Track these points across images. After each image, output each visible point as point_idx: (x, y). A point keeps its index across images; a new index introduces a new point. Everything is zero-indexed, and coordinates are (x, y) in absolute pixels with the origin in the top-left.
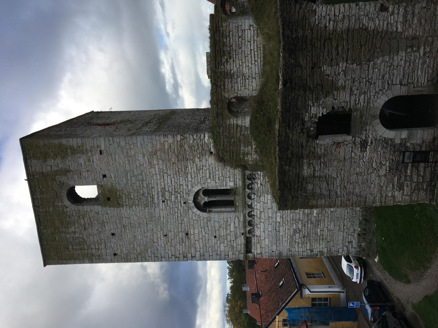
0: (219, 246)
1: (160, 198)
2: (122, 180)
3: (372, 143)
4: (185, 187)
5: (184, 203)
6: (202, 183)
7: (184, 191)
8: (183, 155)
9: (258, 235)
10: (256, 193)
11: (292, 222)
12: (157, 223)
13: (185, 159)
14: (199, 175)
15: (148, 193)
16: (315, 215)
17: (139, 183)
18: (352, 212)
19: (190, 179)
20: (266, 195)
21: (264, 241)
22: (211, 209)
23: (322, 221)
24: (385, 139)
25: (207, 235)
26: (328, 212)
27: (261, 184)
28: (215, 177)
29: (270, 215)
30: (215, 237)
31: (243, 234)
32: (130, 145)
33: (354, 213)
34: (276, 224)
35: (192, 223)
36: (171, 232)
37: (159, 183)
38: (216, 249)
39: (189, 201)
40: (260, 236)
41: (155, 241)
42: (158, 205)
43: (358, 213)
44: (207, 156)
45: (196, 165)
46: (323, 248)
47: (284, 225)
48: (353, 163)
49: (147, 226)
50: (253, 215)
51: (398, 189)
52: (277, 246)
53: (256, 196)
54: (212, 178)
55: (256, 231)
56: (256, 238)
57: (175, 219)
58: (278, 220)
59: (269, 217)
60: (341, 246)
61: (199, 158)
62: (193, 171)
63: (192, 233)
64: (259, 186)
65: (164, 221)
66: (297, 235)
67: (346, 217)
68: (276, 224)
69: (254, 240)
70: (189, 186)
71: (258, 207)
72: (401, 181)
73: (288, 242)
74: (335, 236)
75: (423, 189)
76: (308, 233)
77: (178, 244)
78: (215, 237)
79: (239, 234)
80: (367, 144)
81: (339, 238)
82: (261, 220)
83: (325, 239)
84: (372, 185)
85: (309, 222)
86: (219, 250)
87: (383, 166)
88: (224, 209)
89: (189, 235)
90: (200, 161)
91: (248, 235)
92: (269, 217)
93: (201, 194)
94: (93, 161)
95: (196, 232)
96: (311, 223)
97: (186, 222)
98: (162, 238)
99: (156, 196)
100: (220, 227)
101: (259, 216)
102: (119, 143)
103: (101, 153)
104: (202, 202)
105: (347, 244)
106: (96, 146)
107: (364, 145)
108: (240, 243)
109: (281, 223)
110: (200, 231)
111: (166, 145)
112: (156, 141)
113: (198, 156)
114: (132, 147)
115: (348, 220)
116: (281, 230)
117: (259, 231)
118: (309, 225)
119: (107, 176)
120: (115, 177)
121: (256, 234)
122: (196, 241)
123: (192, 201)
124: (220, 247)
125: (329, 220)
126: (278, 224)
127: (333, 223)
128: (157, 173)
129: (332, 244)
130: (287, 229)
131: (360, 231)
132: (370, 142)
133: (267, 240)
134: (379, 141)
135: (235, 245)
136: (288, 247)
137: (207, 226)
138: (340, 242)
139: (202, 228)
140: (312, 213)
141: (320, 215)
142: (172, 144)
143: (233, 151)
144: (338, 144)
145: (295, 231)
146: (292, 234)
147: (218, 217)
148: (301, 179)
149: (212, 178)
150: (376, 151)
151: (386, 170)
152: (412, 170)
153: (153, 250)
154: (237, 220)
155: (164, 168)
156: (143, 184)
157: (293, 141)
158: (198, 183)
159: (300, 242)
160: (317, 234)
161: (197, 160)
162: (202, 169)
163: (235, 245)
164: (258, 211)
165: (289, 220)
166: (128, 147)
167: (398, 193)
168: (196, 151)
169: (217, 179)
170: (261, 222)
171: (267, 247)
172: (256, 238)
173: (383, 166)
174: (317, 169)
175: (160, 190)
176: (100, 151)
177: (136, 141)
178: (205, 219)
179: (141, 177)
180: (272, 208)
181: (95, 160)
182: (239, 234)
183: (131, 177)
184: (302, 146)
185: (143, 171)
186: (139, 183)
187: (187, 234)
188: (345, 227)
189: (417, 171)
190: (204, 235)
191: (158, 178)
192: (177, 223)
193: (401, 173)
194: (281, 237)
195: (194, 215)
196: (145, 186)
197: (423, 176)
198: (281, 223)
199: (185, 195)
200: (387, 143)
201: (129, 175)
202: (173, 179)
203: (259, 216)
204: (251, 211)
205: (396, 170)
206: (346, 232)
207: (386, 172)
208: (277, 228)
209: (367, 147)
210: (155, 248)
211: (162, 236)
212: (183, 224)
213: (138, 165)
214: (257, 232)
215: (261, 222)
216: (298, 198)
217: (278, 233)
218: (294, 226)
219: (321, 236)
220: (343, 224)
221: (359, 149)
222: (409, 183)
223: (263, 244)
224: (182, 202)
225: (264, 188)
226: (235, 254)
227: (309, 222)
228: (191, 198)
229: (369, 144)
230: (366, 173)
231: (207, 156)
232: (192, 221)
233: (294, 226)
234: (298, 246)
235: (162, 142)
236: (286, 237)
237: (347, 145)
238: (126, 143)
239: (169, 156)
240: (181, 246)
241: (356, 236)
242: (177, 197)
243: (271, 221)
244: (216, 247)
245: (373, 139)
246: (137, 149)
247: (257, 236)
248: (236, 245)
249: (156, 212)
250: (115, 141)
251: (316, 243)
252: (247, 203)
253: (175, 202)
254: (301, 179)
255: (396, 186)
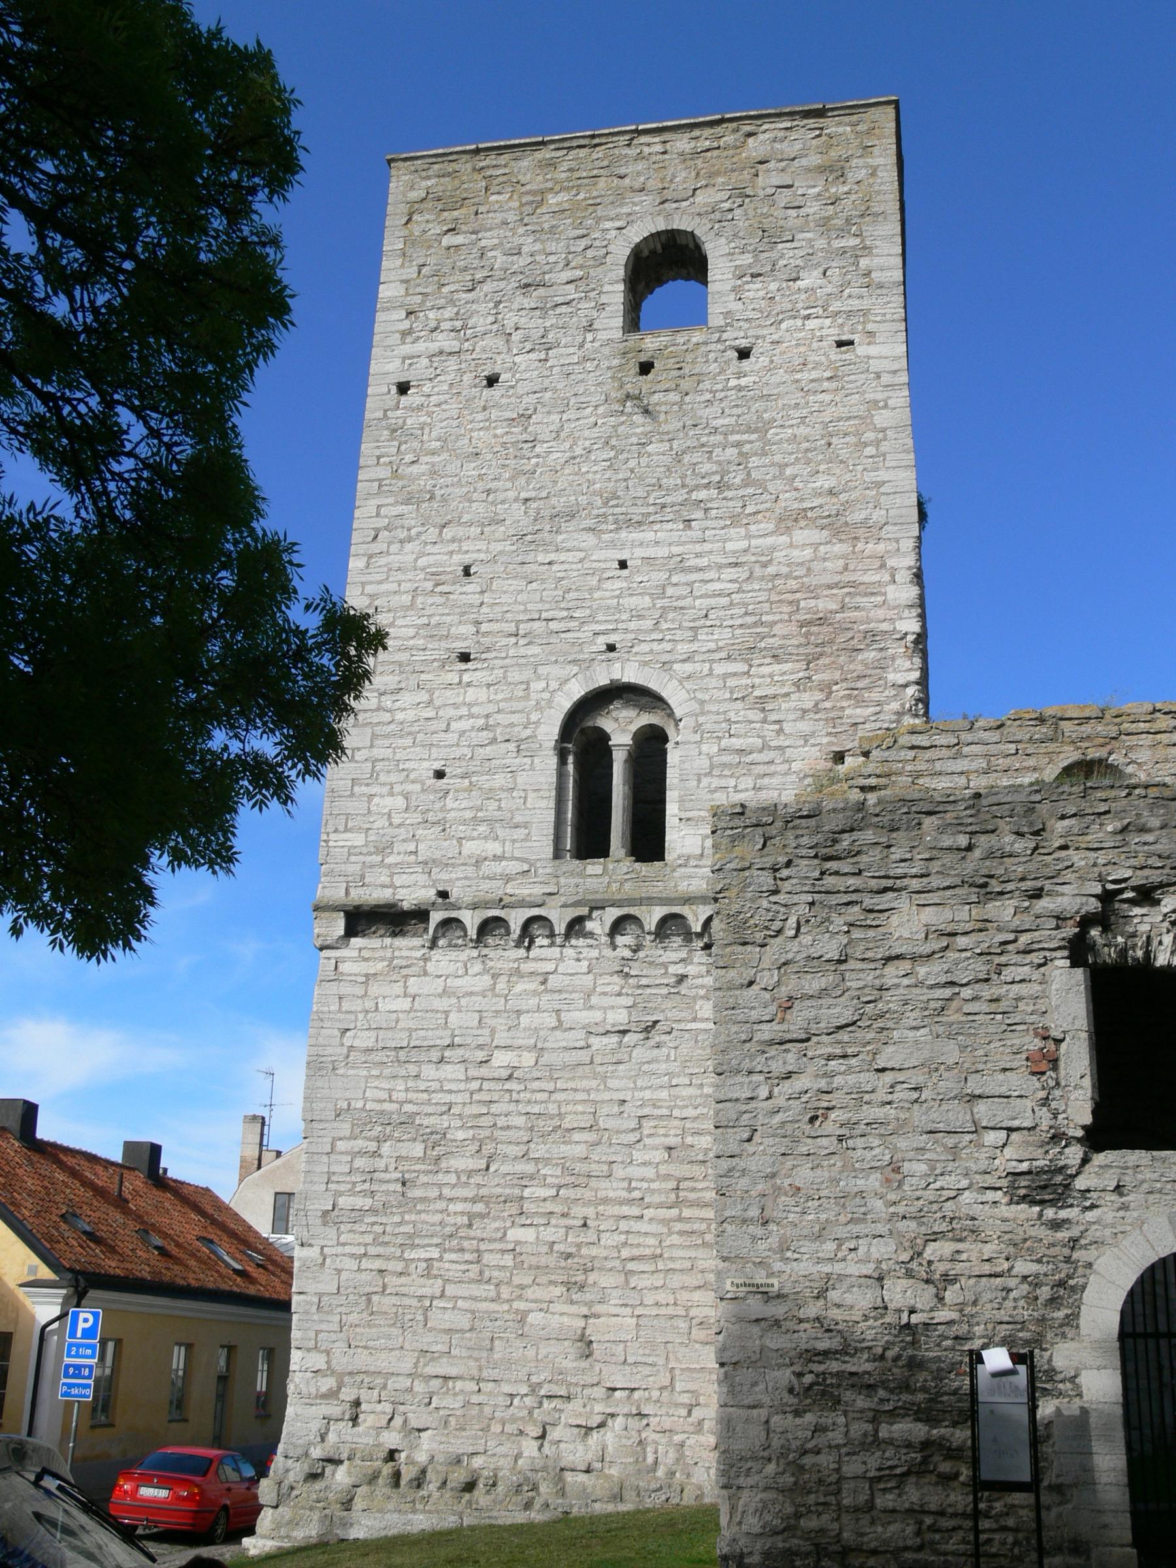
0: (397, 788)
1: (640, 552)
2: (727, 411)
3: (1056, 1225)
4: (683, 648)
5: (611, 648)
6: (701, 719)
7: (668, 646)
8: (831, 642)
9: (430, 967)
10: (641, 954)
11: (486, 1121)
12: (529, 538)
13: (810, 649)
14: (739, 705)
15: (664, 506)
16: (514, 1234)
17: (713, 473)
18: (514, 1419)
19: (720, 669)
20: (629, 1001)
21: (400, 991)
22: (571, 759)
23: (475, 1268)
24: (1073, 1289)
25: (452, 737)
26: (520, 1297)
27: (682, 978)
28: (726, 772)
29: (525, 1020)
30: (440, 775)
31: (444, 895)
32: (877, 443)
33: (509, 1428)
34: (480, 1047)
35: (515, 676)
36: (482, 592)
37: (707, 547)
38: (383, 778)
39: (618, 665)
40: (425, 974)
41: (448, 533)
42: (612, 545)
43: (507, 1448)
44: (825, 740)
45: (787, 695)
46: (339, 1271)
47: (475, 1085)
48: (950, 1141)
49: (516, 500)
50: (531, 942)
51: (808, 1379)
52: (368, 1050)
53: (627, 953)
54: (726, 758)
55: (453, 954)
56: (419, 954)
57: (540, 606)
58: (501, 1059)
59: (519, 1013)
60: (341, 1361)
61: (816, 708)
62: (757, 681)
63: (466, 678)
64: (672, 969)
65: (534, 567)
66: (418, 1150)
67: (487, 1387)
68: (480, 1047)
69: (409, 946)
70: (688, 668)
71: (569, 966)
72: (848, 1396)
73: (387, 1106)
74: (395, 1331)
75: (798, 1516)
76: (423, 1200)
77: (425, 620)
78: (440, 775)
79: (444, 876)
80: (1052, 1203)
81: (384, 1355)
82: (503, 979)
83: (384, 1287)
84: (831, 1246)
85: (479, 1207)
86: (374, 790)
87: (932, 1290)
88: (570, 815)
89: (463, 666)
90: (804, 711)
91: (436, 917)
92: (519, 1013)
93: (646, 719)
94: (808, 317)
95: (471, 694)
96: (471, 1216)
97: (522, 651)
98: (456, 558)
99: (649, 536)
100: (490, 794)
101: (527, 967)
102: (886, 406)
103: (840, 344)
104: (606, 723)
105: (348, 1394)
106: (870, 327)
107: (1045, 1188)
108: (398, 880)
109: (484, 1071)
110: (475, 710)
111: (877, 578)
112: (897, 541)
113: (828, 705)
114: (870, 451)
115: (475, 1399)
116: (448, 1071)
117: (452, 968)
118: (459, 1207)
119: (745, 362)
120: (740, 388)
121: (436, 954)
122: (431, 692)
123: (616, 676)
124: (391, 794)
125: (484, 1306)
126: (481, 1055)
127: (464, 1322)
128: (754, 542)
129: (354, 1318)
130: (448, 1098)
131: (410, 1461)
132: (1063, 1214)
133: (405, 1004)
134: (1068, 1260)
135: (390, 860)
136: (360, 1105)
137: (494, 741)
138: (362, 1360)
139: (487, 716)
140: (523, 1220)
141: (508, 1260)
142: (880, 599)
143: (885, 787)
144: (1046, 1062)
145: (436, 1139)
146: (426, 1121)
147: (536, 786)
148: (868, 901)
149: (726, 758)
150: (1018, 1246)
151: (912, 1311)
152: (909, 1445)
153: (407, 523)
154: (513, 867)
155: (771, 570)
156: (707, 486)
157: (1063, 853)
158: (702, 703)
159: (380, 1164)
160: (413, 1246)
161: (808, 699)
162: (764, 721)
163: (390, 860)
164: (550, 967)
165: (494, 1108)
166: (870, 436)
167: (784, 1383)
168: (849, 697)
169: (716, 782)
170: (495, 976)
171: (369, 1005)
172: (419, 954)
173: (932, 1290)
174: (922, 971)
175: (676, 550)
176: (851, 343)
177: (894, 464)
178: (528, 732)
179: (738, 481)
180: (560, 1026)
181: (812, 324)
182: (444, 876)
183: (738, 444)
184: (1037, 894)
185: (766, 489)
186: (713, 473)
187: (465, 658)
188: (436, 1383)
189: (903, 1475)
190: (454, 726)
191: (730, 546)
192: (521, 617)
193: (892, 1391)
194: (412, 1069)
195: (554, 685)
196: (702, 494)
197: (870, 1506)
198: (484, 1071)
199: (645, 647)
200: (1053, 1302)
201: (745, 437)
202: (724, 601)
203: (527, 967)
204: (552, 935)
205: (912, 1358)
206: (410, 1390)
207: (900, 1311)
208: (460, 1052)
209: (1033, 1202)
210: (413, 532)
211: (467, 559)
212: (513, 640)
213: (789, 471)
214: (445, 960)
215: (495, 976)
216: (776, 892)
217: (435, 1055)
218: (461, 1135)
219: (400, 1266)
220: (453, 1372)
221: (1024, 1166)
222: (837, 1437)
223: (386, 989)
224: (612, 639)
225: (665, 991)
226: (347, 861)
227: (479, 1207)
228: (630, 674)
229: (1050, 1213)
230: (900, 1209)
231: (825, 740)
232: (527, 674)
233: (461, 1135)
234: (361, 1153)
235: (891, 563)
236: (411, 1096)
237: (1045, 1102)
238: (883, 430)
239: (830, 587)
240: (412, 632)
241: (391, 1439)
242: (640, 617)
243: (500, 1023)
244: (393, 778)
245: (1075, 1232)
246: (860, 468)
247: (426, 959)
248: (389, 866)
249: (576, 535)
250: (890, 394)
251: (369, 1239)
252: (595, 914)
253: (618, 609)
254: (868, 901)
255: (821, 1368)
